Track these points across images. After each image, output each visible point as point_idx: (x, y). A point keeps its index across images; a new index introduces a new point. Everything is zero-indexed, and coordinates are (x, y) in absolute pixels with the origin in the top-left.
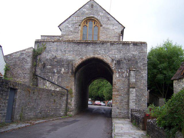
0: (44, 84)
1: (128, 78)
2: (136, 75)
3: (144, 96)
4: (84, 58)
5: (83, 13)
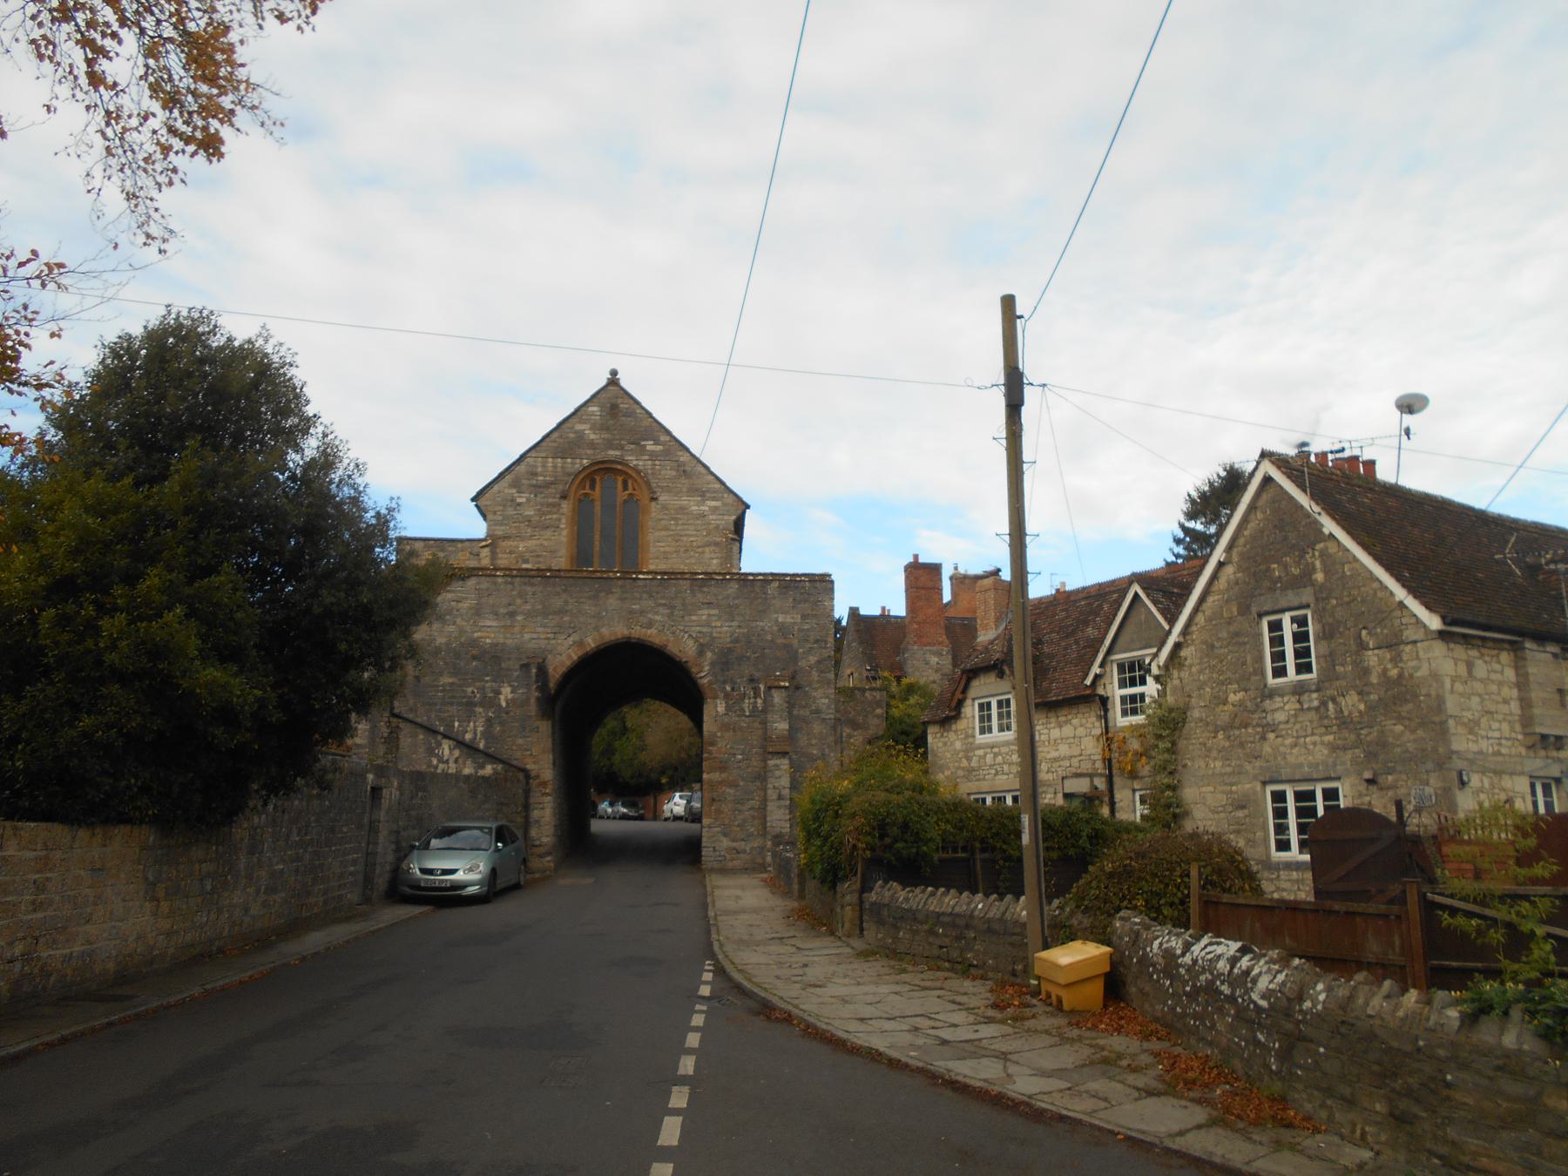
0: (431, 752)
1: (761, 715)
4: (591, 643)
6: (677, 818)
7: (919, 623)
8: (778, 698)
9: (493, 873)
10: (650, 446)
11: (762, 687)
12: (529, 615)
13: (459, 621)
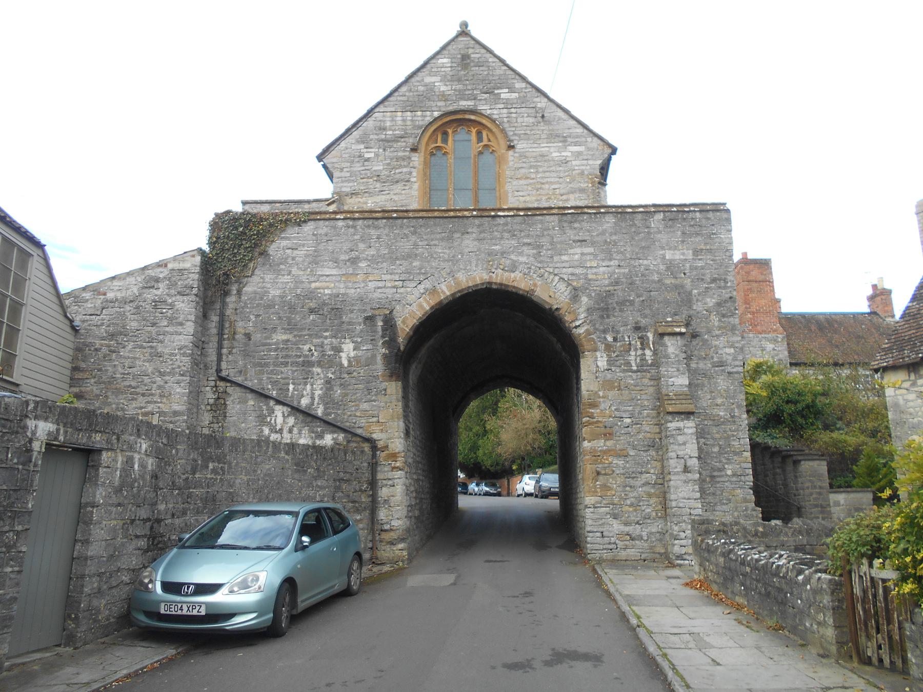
0: (262, 420)
1: (652, 370)
2: (689, 358)
3: (735, 453)
4: (446, 290)
5: (430, 93)
6: (528, 495)
7: (753, 313)
8: (672, 346)
9: (289, 585)
10: (504, 94)
11: (650, 336)
12: (373, 261)
13: (294, 271)
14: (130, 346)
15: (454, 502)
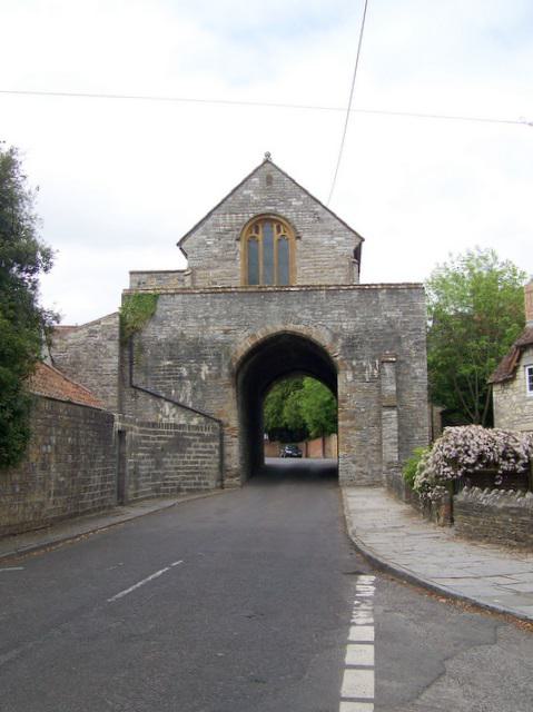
0: (157, 410)
1: (376, 381)
4: (260, 335)
5: (246, 202)
14: (83, 370)
15: (263, 460)
